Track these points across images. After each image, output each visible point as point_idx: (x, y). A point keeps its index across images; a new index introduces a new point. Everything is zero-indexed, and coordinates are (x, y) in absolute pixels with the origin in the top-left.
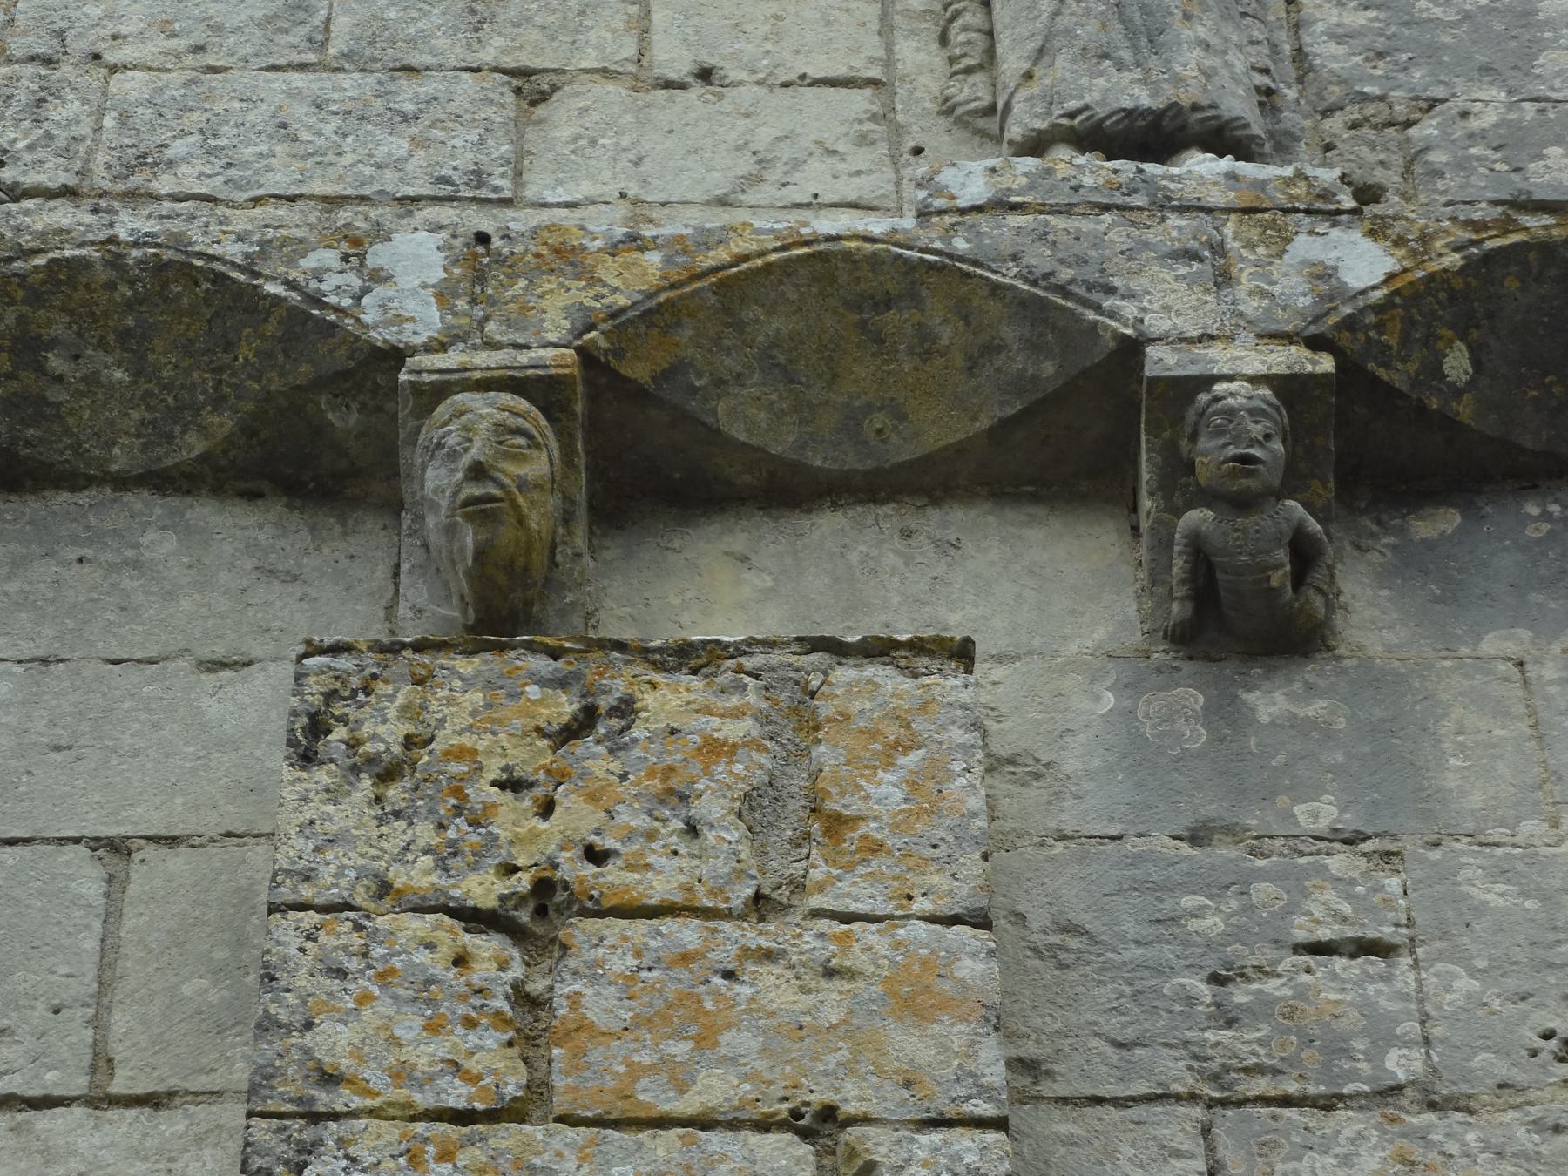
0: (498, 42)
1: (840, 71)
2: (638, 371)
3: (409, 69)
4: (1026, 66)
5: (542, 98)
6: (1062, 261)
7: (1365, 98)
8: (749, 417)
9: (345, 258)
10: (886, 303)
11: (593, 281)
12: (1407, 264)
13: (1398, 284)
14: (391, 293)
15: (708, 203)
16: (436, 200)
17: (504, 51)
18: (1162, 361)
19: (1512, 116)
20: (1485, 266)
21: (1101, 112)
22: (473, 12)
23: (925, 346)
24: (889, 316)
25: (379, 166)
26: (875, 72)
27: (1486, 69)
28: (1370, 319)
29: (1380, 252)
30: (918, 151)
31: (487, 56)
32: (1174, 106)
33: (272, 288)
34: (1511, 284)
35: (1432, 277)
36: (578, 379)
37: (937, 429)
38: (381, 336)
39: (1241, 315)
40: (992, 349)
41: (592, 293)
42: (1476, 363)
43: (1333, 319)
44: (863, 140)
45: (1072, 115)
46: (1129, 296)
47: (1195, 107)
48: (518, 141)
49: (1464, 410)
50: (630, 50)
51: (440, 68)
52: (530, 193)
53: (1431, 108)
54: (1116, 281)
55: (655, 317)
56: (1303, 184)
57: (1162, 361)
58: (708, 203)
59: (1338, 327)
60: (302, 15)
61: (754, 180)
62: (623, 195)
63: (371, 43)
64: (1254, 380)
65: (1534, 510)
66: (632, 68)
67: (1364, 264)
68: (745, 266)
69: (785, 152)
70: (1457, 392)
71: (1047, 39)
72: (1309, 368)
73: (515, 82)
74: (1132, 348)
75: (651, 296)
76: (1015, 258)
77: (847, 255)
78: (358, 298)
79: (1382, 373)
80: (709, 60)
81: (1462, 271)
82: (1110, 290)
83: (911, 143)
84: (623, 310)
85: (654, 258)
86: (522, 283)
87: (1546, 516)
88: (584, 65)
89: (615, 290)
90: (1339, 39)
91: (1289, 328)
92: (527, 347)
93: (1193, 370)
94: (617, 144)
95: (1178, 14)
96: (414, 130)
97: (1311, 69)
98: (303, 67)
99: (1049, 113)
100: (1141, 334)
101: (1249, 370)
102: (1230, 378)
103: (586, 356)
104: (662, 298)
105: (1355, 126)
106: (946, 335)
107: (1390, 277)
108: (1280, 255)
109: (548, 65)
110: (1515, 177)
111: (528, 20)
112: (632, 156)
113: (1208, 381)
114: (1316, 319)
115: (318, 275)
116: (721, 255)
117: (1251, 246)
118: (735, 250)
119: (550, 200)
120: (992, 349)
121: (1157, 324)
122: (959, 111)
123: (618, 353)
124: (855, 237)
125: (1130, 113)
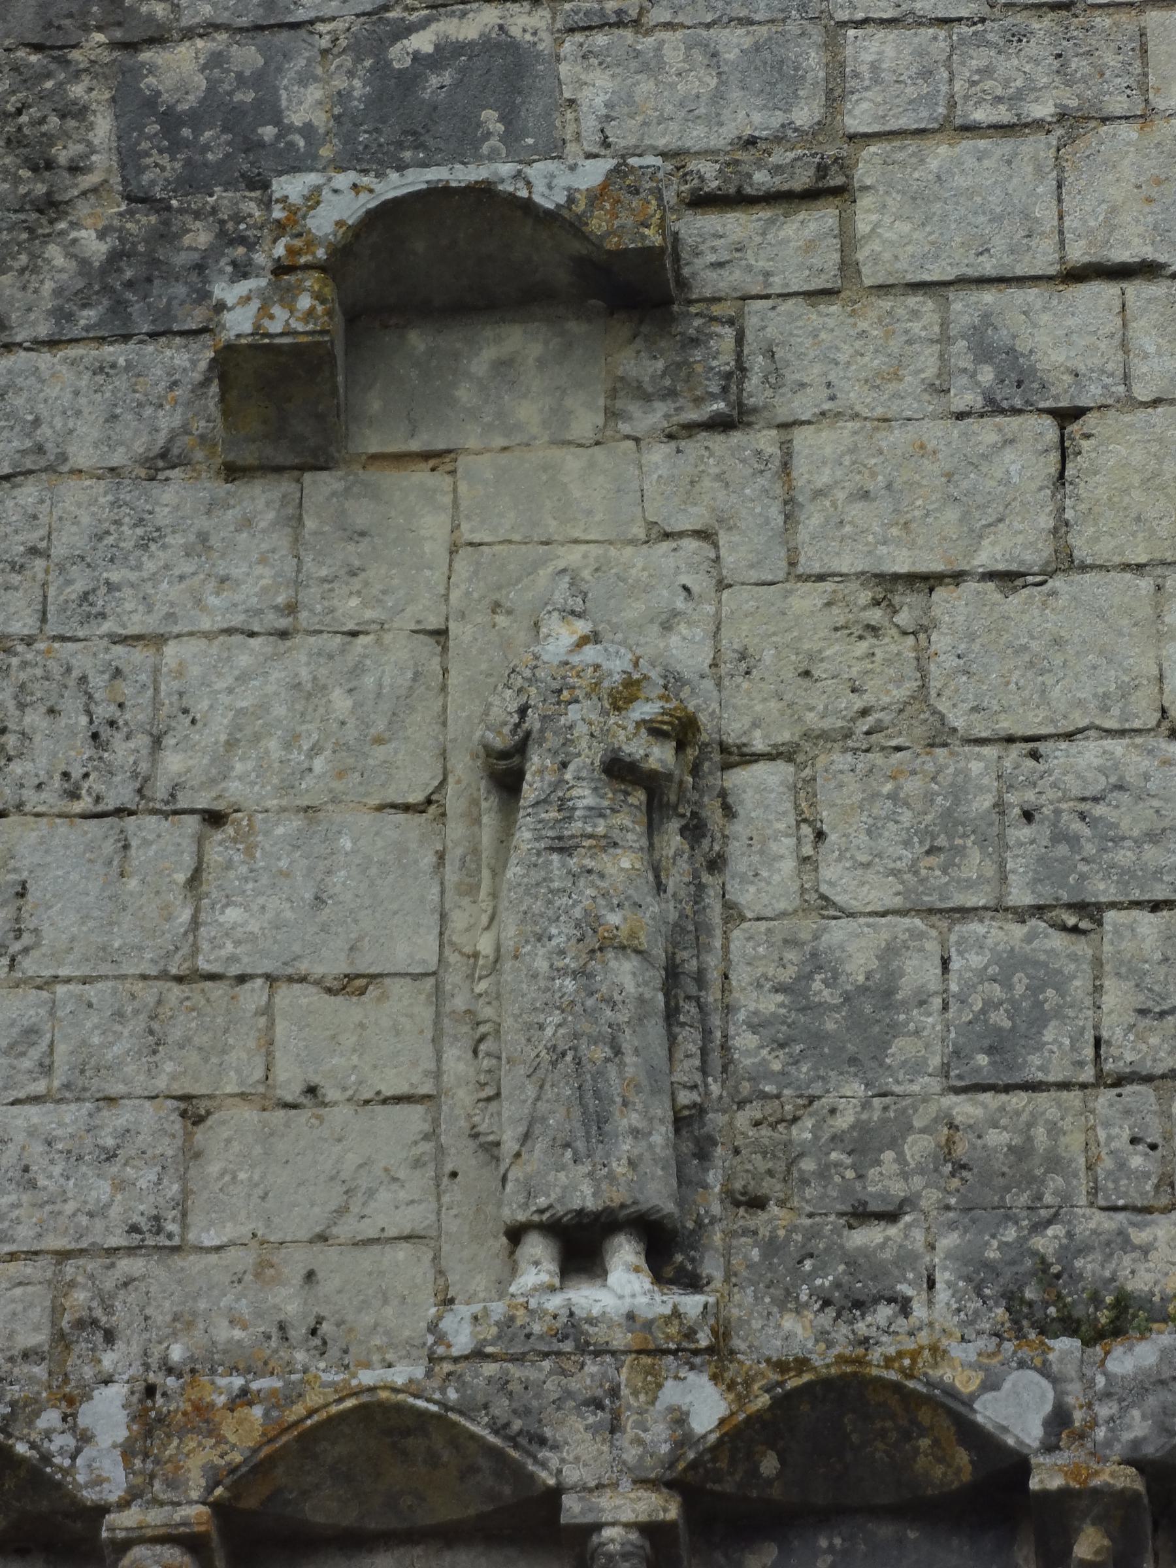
0: (169, 1067)
1: (403, 1089)
2: (250, 1503)
3: (110, 1100)
4: (517, 1147)
5: (199, 1120)
6: (515, 1412)
7: (765, 1096)
8: (325, 1509)
9: (64, 1419)
10: (408, 1432)
11: (221, 1440)
12: (734, 1407)
13: (725, 1429)
14: (95, 1454)
15: (311, 1242)
16: (131, 1251)
17: (174, 1077)
18: (573, 1508)
19: (864, 1117)
20: (785, 1402)
21: (560, 1210)
22: (151, 1032)
23: (433, 1460)
24: (411, 1440)
25: (91, 1215)
26: (426, 1088)
27: (853, 1061)
28: (707, 1457)
29: (717, 1397)
30: (454, 1175)
31: (161, 1084)
32: (607, 1209)
33: (21, 1448)
34: (805, 1408)
35: (749, 1418)
36: (215, 1536)
37: (445, 1511)
38: (90, 1496)
39: (624, 1463)
40: (473, 1469)
41: (219, 1451)
42: (782, 1461)
43: (681, 1466)
44: (417, 1163)
45: (541, 1212)
46: (555, 1447)
47: (623, 1206)
48: (183, 1179)
49: (776, 1492)
50: (259, 1074)
51: (129, 1096)
52: (191, 1237)
53: (811, 1103)
54: (548, 1432)
55: (259, 1468)
56: (676, 1322)
57: (573, 1508)
58: (311, 1242)
59: (685, 1470)
60: (34, 1037)
61: (342, 1211)
62: (254, 1235)
63: (82, 1072)
64: (627, 1525)
65: (823, 1543)
66: (261, 1089)
67: (705, 1406)
68: (316, 1418)
69: (364, 1183)
70: (769, 1482)
71: (530, 1126)
72: (661, 1516)
73: (183, 1106)
74: (554, 1495)
75: (255, 1451)
76: (486, 1406)
77: (381, 1404)
78: (73, 1458)
79: (717, 1487)
80: (315, 1080)
81: (771, 1408)
82: (542, 1441)
83: (449, 1167)
84: (238, 1467)
85: (257, 1411)
86: (175, 1442)
87: (831, 1549)
88: (228, 1090)
89: (233, 1447)
90: (754, 1028)
91: (653, 1476)
92: (179, 1504)
93: (589, 1518)
94: (250, 1179)
95: (618, 1100)
96: (114, 1170)
97: (731, 1061)
98: (36, 1099)
99: (525, 1206)
100: (559, 1484)
101: (624, 1519)
102: (613, 1524)
103: (218, 1508)
104: (262, 1454)
105: (757, 1124)
106: (446, 1456)
107: (722, 1422)
108: (653, 1402)
109: (203, 1091)
110: (858, 1186)
111: (189, 1040)
112: (259, 1191)
113: (598, 1527)
114: (672, 1465)
115: (48, 1434)
116: (299, 1410)
117: (635, 1393)
118: (310, 1404)
119: (207, 1243)
120: (473, 1469)
121: (572, 1475)
122: (482, 1139)
123: (237, 1497)
124: (385, 1388)
125: (581, 1212)
